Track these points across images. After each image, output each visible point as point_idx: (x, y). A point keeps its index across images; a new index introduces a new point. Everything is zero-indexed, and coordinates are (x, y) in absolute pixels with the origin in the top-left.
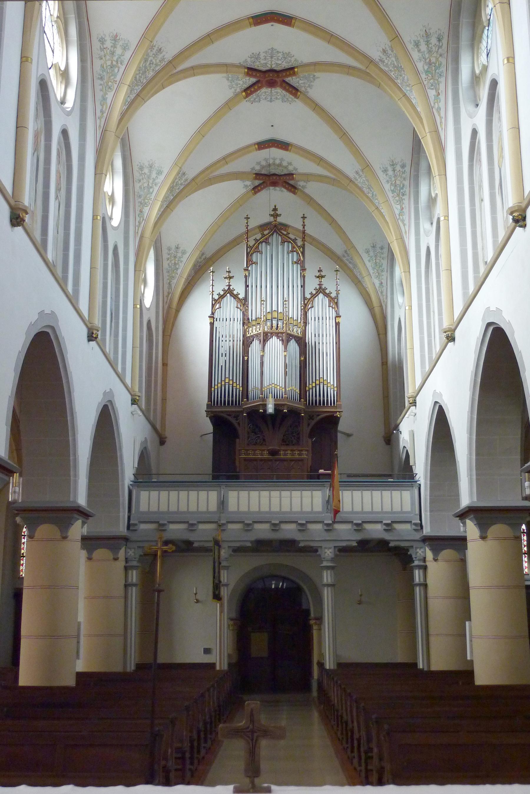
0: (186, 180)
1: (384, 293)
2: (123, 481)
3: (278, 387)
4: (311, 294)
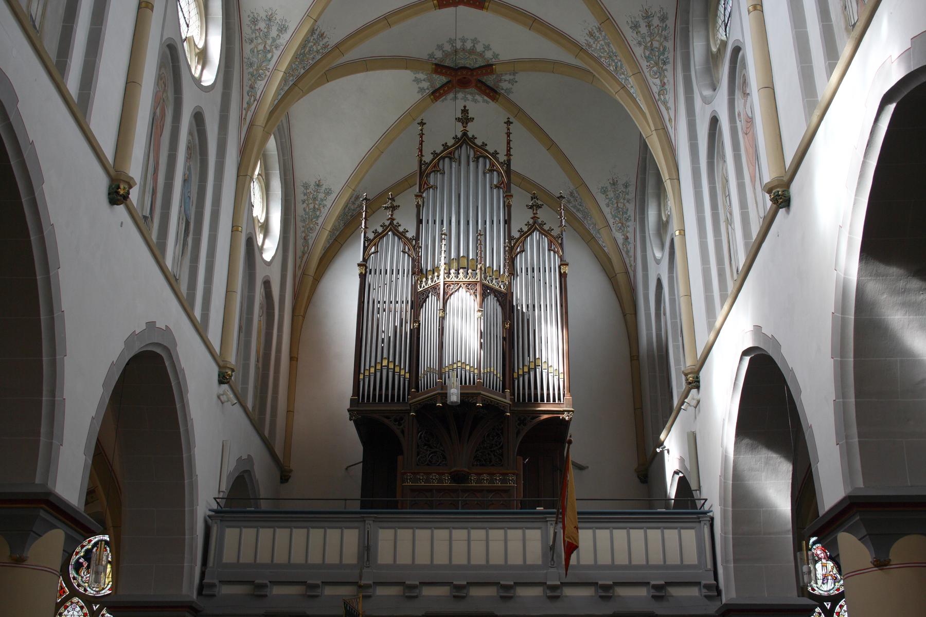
0: (325, 46)
1: (632, 253)
2: (193, 504)
3: (468, 368)
4: (521, 231)
